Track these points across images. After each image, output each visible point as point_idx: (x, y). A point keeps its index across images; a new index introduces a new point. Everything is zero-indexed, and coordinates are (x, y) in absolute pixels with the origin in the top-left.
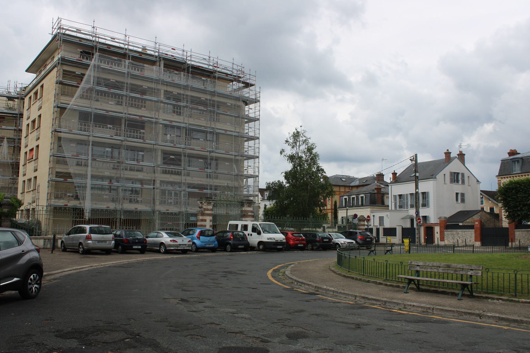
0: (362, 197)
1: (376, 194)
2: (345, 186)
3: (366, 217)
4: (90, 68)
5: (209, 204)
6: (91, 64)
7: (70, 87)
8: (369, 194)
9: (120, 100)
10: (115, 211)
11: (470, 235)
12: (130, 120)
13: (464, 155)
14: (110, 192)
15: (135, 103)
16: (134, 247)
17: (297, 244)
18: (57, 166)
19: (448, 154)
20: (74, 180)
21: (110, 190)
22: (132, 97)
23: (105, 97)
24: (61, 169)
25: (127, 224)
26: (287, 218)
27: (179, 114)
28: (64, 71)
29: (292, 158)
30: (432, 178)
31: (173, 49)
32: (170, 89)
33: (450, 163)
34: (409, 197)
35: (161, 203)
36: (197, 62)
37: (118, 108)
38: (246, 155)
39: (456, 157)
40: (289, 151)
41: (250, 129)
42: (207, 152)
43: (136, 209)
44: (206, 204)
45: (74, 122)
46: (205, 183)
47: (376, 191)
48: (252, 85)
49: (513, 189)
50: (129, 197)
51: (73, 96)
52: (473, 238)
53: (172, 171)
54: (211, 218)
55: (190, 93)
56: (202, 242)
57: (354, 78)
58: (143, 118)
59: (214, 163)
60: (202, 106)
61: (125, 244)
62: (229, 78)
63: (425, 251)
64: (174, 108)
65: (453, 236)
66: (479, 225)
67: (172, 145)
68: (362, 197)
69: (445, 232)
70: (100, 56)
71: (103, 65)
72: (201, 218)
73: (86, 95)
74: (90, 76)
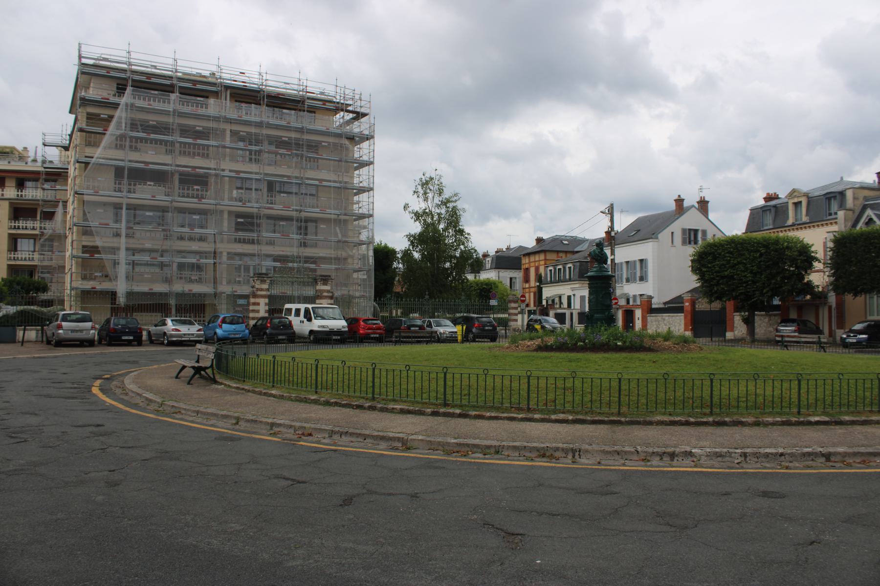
0: (570, 268)
1: (589, 263)
2: (566, 252)
3: (519, 296)
4: (120, 107)
5: (263, 282)
6: (122, 103)
7: (98, 135)
8: (578, 264)
10: (166, 295)
11: (678, 321)
12: (181, 174)
13: (708, 202)
14: (162, 270)
15: (185, 150)
16: (124, 338)
17: (369, 334)
18: (84, 238)
19: (679, 201)
20: (103, 256)
21: (162, 268)
22: (185, 143)
23: (151, 145)
24: (87, 241)
26: (387, 299)
27: (257, 161)
28: (88, 114)
29: (417, 216)
30: (652, 238)
32: (235, 128)
33: (682, 215)
34: (624, 266)
35: (229, 283)
36: (284, 88)
37: (167, 159)
38: (356, 213)
39: (693, 206)
40: (419, 205)
41: (361, 177)
42: (293, 211)
43: (190, 290)
44: (258, 282)
45: (106, 181)
46: (289, 254)
47: (589, 259)
48: (364, 115)
49: (710, 254)
50: (189, 276)
51: (98, 146)
52: (683, 326)
53: (244, 240)
54: (267, 300)
55: (265, 131)
56: (224, 331)
57: (681, 80)
58: (197, 170)
59: (311, 225)
60: (283, 149)
61: (112, 334)
62: (329, 106)
65: (657, 323)
66: (690, 307)
67: (240, 204)
68: (570, 268)
69: (648, 318)
70: (133, 91)
71: (140, 103)
72: (252, 300)
73: (120, 142)
74: (120, 118)
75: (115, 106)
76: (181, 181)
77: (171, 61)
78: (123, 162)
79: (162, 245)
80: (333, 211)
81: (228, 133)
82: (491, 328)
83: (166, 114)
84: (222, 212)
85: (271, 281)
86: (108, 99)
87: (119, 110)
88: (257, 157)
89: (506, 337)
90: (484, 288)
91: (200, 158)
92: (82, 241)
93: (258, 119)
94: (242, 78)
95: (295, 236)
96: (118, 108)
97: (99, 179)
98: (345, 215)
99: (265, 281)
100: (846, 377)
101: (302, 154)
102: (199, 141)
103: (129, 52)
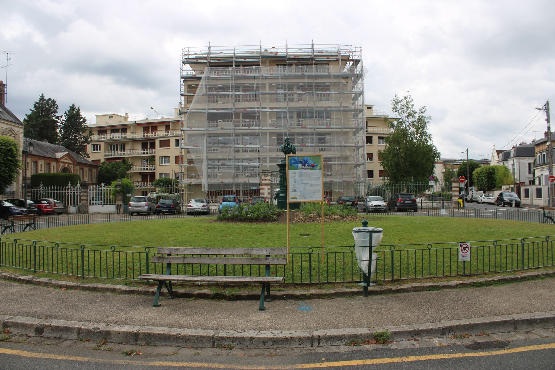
4: (202, 79)
5: (266, 175)
9: (238, 98)
22: (212, 95)
25: (212, 194)
27: (291, 100)
31: (274, 47)
37: (230, 105)
44: (263, 176)
63: (123, 218)
64: (209, 98)
67: (273, 127)
74: (202, 85)
75: (199, 79)
76: (244, 118)
77: (259, 47)
78: (205, 110)
79: (229, 156)
80: (335, 127)
81: (267, 85)
82: (411, 202)
83: (227, 79)
84: (266, 133)
85: (271, 174)
86: (196, 76)
87: (201, 81)
88: (216, 99)
89: (422, 209)
90: (491, 172)
91: (248, 102)
92: (187, 156)
93: (283, 74)
94: (274, 50)
95: (310, 145)
96: (200, 80)
97: (192, 121)
98: (344, 128)
99: (267, 175)
100: (397, 248)
101: (313, 92)
102: (248, 93)
103: (210, 47)
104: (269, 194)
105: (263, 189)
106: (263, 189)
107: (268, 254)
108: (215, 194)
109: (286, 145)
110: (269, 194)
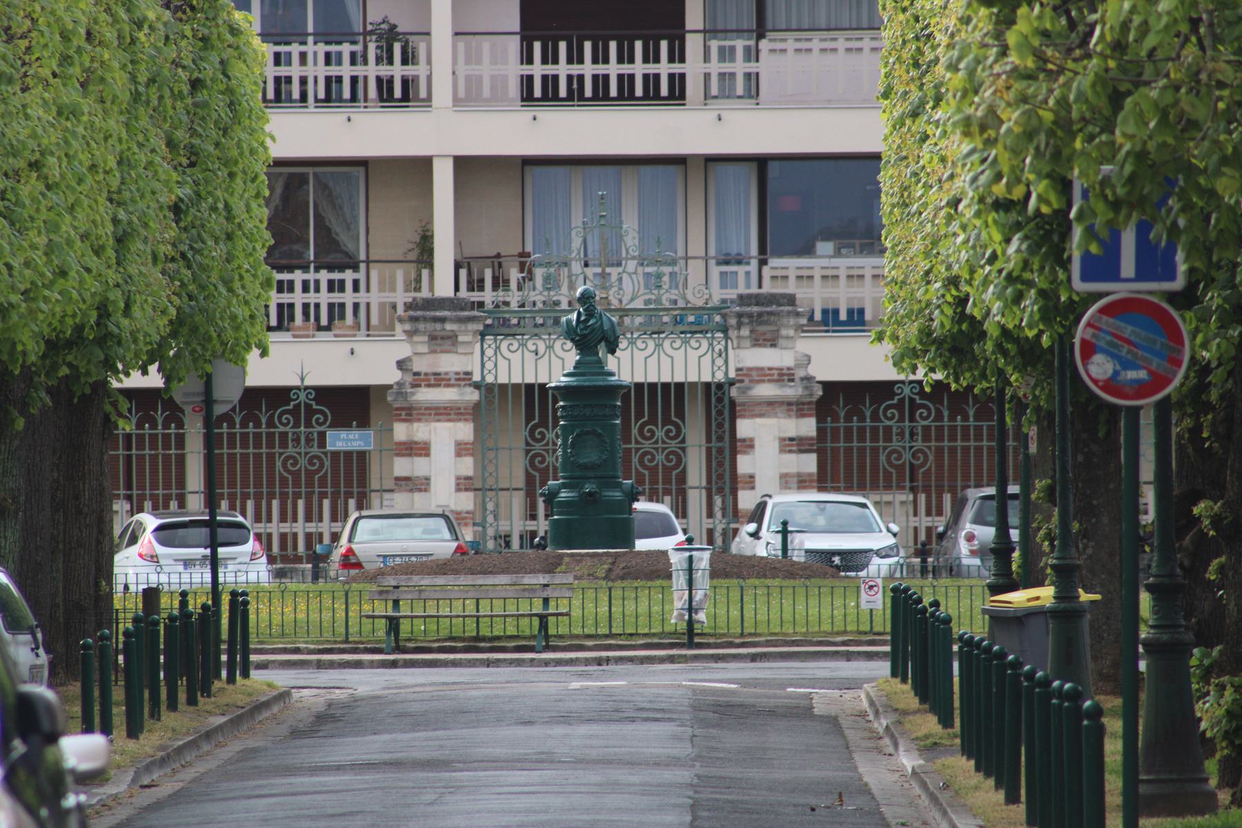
99: (453, 338)
104: (463, 484)
105: (419, 449)
106: (419, 449)
107: (546, 582)
108: (271, 484)
109: (583, 318)
110: (463, 484)
